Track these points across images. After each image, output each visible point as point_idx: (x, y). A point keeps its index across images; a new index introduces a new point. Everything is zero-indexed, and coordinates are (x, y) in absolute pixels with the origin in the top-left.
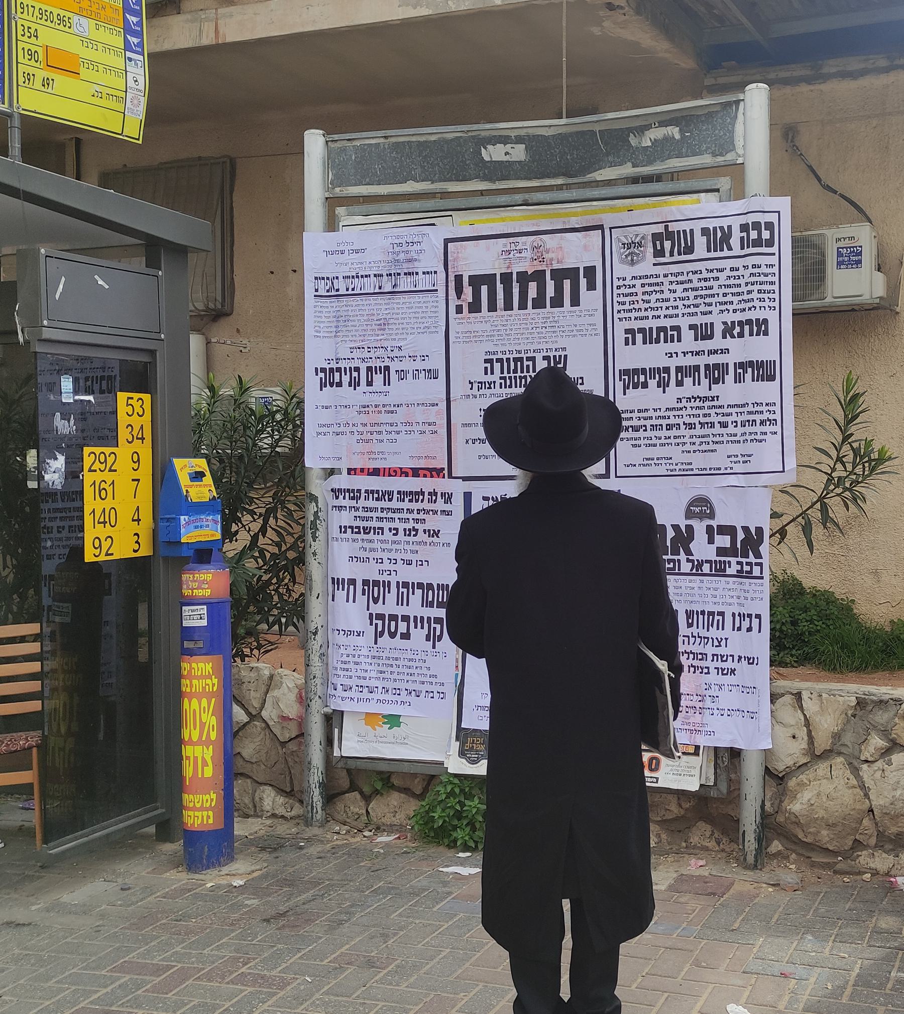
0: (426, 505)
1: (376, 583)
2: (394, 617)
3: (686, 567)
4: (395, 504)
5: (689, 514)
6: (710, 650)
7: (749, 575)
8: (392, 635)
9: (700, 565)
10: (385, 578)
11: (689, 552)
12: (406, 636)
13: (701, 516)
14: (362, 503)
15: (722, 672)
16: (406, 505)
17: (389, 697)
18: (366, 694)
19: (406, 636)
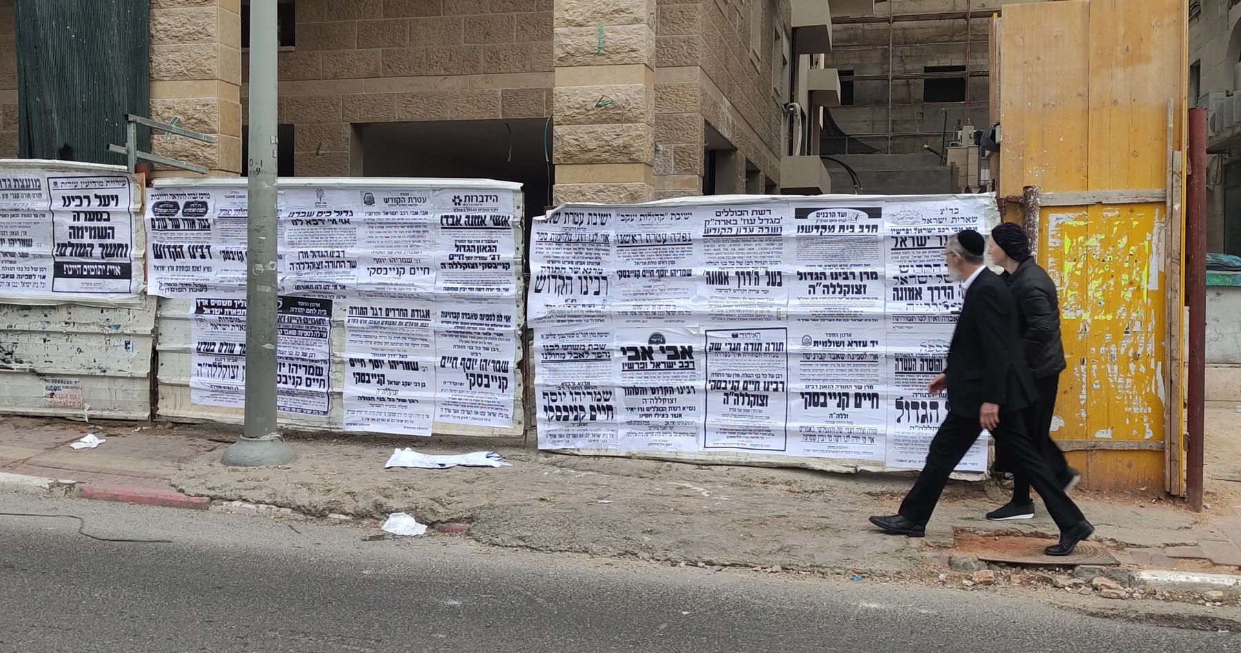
0: (496, 322)
1: (469, 360)
2: (480, 376)
3: (650, 366)
4: (478, 321)
5: (650, 342)
6: (667, 405)
7: (687, 368)
8: (480, 385)
9: (658, 365)
10: (474, 357)
11: (651, 358)
12: (487, 386)
13: (657, 343)
14: (460, 320)
15: (675, 416)
16: (485, 322)
17: (478, 416)
18: (466, 415)
19: (487, 386)
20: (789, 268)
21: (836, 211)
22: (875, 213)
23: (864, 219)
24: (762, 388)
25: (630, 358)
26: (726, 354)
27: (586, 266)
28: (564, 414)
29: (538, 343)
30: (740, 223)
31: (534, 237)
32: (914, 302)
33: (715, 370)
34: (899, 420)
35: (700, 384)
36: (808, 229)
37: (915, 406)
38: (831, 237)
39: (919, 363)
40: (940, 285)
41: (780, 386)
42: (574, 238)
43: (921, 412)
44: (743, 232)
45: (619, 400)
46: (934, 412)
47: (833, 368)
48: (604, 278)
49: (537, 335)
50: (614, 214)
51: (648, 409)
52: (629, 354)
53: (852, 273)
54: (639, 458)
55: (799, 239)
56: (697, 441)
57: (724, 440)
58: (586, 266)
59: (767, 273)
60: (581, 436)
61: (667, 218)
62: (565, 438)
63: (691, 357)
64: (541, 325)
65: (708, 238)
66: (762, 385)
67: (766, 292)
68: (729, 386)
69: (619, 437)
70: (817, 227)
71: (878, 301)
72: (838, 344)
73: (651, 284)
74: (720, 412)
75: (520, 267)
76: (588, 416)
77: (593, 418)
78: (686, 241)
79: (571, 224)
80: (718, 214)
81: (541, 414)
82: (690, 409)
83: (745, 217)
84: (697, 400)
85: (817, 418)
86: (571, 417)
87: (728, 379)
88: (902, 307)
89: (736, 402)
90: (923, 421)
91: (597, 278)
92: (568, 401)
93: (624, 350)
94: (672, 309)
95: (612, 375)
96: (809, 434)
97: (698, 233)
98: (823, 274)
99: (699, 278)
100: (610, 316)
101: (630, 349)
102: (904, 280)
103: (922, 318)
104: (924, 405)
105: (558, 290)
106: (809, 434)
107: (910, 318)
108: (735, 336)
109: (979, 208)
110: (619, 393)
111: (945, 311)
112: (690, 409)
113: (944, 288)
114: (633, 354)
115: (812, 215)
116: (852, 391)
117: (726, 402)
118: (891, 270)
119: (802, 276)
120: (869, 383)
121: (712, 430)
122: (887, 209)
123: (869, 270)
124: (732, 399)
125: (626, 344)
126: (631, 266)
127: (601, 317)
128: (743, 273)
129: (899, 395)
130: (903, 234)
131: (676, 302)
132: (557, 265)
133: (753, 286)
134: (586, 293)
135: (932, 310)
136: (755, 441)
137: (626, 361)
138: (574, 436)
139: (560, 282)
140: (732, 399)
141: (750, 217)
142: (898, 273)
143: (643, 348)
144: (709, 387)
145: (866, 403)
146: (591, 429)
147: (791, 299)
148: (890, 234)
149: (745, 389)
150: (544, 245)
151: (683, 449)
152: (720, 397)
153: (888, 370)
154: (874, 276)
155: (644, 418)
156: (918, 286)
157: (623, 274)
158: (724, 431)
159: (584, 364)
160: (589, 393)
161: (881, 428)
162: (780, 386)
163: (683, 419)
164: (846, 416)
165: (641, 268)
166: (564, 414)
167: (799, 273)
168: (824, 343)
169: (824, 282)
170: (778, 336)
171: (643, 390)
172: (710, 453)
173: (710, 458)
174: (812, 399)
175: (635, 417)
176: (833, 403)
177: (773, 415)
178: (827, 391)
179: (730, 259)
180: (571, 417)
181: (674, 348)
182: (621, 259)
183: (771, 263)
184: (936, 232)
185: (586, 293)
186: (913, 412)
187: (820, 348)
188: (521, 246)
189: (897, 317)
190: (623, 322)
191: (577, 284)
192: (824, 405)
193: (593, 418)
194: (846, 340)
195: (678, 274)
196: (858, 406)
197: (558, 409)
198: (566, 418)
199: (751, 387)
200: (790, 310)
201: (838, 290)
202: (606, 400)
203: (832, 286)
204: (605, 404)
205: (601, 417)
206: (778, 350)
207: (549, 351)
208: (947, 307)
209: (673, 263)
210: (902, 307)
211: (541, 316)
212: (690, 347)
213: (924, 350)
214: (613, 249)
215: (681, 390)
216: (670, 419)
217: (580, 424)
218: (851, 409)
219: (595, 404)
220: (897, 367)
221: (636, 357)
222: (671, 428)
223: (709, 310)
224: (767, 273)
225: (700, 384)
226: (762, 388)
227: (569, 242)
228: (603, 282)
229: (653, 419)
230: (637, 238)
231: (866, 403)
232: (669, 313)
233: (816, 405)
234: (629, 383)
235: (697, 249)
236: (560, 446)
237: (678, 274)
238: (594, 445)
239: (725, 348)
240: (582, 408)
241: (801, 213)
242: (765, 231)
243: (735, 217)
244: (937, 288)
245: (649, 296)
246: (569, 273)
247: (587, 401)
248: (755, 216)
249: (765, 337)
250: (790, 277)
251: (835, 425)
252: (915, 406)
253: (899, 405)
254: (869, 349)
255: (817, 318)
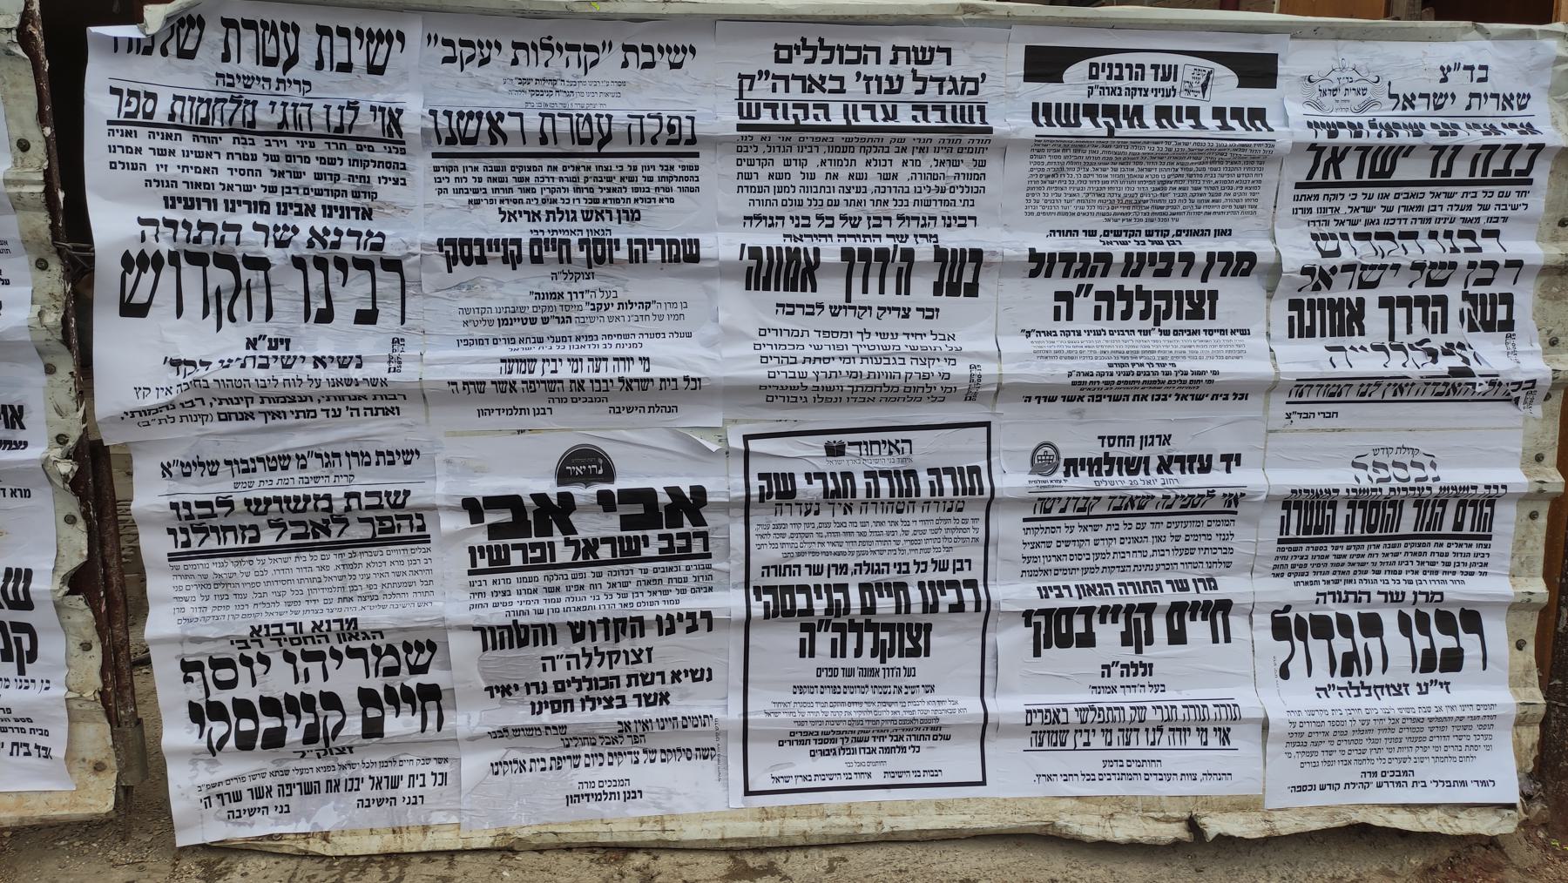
3: (564, 554)
5: (563, 476)
6: (622, 669)
9: (591, 546)
11: (568, 529)
13: (587, 479)
15: (647, 700)
20: (1006, 236)
21: (1147, 60)
22: (1258, 71)
23: (1227, 90)
24: (916, 608)
25: (495, 531)
26: (810, 508)
27: (319, 222)
28: (267, 723)
29: (149, 495)
30: (855, 90)
31: (99, 105)
32: (1345, 341)
33: (773, 556)
34: (1284, 673)
35: (729, 601)
36: (1068, 114)
37: (1322, 628)
38: (1136, 141)
39: (1342, 512)
40: (1412, 293)
41: (968, 594)
42: (266, 116)
43: (1341, 645)
44: (865, 119)
45: (461, 667)
46: (1374, 644)
47: (1111, 535)
48: (393, 265)
49: (145, 469)
50: (415, 33)
51: (560, 686)
52: (491, 518)
53: (1188, 258)
54: (540, 850)
55: (1039, 146)
56: (722, 775)
57: (802, 763)
58: (319, 222)
59: (940, 254)
60: (333, 786)
61: (611, 61)
62: (275, 799)
63: (698, 521)
64: (156, 432)
65: (759, 136)
66: (915, 595)
67: (930, 313)
68: (820, 605)
69: (473, 784)
70: (1091, 111)
71: (1254, 342)
72: (1133, 466)
73: (561, 286)
74: (785, 680)
75: (42, 221)
76: (354, 726)
77: (373, 729)
78: (679, 142)
79: (248, 65)
80: (783, 54)
81: (177, 735)
82: (697, 675)
83: (870, 69)
84: (719, 650)
85: (1068, 679)
86: (294, 735)
87: (812, 581)
88: (1309, 357)
89: (838, 650)
90: (1347, 672)
91: (363, 264)
92: (279, 681)
93: (474, 508)
94: (636, 371)
95: (440, 591)
96: (1049, 730)
97: (718, 116)
98: (1106, 258)
99: (724, 271)
100: (423, 396)
101: (494, 503)
102: (1326, 278)
103: (1368, 389)
104: (1345, 626)
105: (218, 307)
106: (1049, 730)
107: (1333, 390)
108: (835, 451)
109: (1540, 67)
110: (463, 647)
111: (1430, 368)
112: (697, 675)
113: (1422, 302)
114: (505, 516)
115: (1077, 72)
116: (1166, 597)
117: (807, 650)
118: (1296, 249)
119: (1040, 264)
120: (1202, 572)
121: (765, 736)
122: (1295, 61)
123: (1231, 246)
124: (824, 640)
125: (482, 488)
126: (485, 224)
127: (386, 400)
128: (865, 253)
129: (1281, 600)
130: (1344, 136)
131: (650, 348)
132: (206, 215)
133: (891, 298)
134: (326, 316)
135: (1396, 365)
136: (896, 761)
137: (481, 539)
138: (309, 789)
139: (221, 277)
140: (824, 640)
141: (884, 69)
142: (1312, 257)
143: (540, 498)
144: (758, 610)
145: (1198, 629)
146: (367, 763)
147: (1001, 336)
148: (1309, 136)
149: (869, 610)
150: (142, 139)
151: (686, 806)
152: (790, 635)
153: (1258, 535)
154: (1242, 264)
155: (547, 717)
156: (1353, 295)
157: (460, 252)
158: (798, 738)
159: (333, 559)
160: (353, 653)
161: (1250, 703)
162: (968, 594)
163: (677, 708)
164: (1148, 668)
165: (522, 230)
166: (267, 723)
167: (1034, 256)
168: (1094, 466)
169: (1100, 284)
170: (964, 449)
171: (545, 633)
172: (765, 814)
173: (771, 829)
174: (1054, 629)
175: (518, 714)
176: (1108, 634)
177: (945, 678)
178: (1096, 601)
179: (835, 204)
180: (294, 735)
181: (647, 496)
182: (449, 200)
183: (948, 222)
184: (1432, 136)
185: (326, 316)
186: (1318, 647)
187: (1083, 481)
188: (38, 137)
189: (1301, 387)
190: (466, 416)
191: (288, 287)
192: (1087, 640)
193: (373, 729)
194: (1154, 452)
195: (655, 254)
196: (1178, 637)
197: (244, 709)
198: (275, 739)
199: (885, 604)
200: (1011, 370)
201: (1139, 306)
202: (415, 670)
203: (1123, 294)
204: (412, 682)
205: (399, 724)
206: (969, 489)
207: (194, 523)
208: (1433, 355)
209: (634, 216)
210: (1309, 357)
211: (152, 401)
212: (699, 492)
213: (1365, 479)
214: (421, 165)
215: (667, 625)
216: (633, 712)
217: (328, 751)
218: (1158, 650)
219: (377, 684)
220: (1285, 525)
221: (518, 526)
222: (636, 739)
223: (760, 373)
224: (940, 254)
225: (729, 601)
226: (916, 608)
227: (248, 130)
228: (387, 283)
229: (577, 718)
230: (509, 125)
231: (1198, 629)
232: (627, 384)
233: (1064, 642)
234: (496, 616)
235: (717, 175)
236: (261, 826)
237: (655, 254)
238: (379, 817)
239: (809, 490)
240: (331, 701)
241: (1044, 64)
242: (934, 118)
243: (835, 69)
244: (1405, 302)
245: (555, 328)
246: (253, 242)
247: (348, 679)
248: (903, 68)
249: (927, 451)
250: (1007, 267)
251: (1119, 697)
252: (1322, 628)
253: (1281, 629)
254: (1217, 478)
255: (1084, 392)
